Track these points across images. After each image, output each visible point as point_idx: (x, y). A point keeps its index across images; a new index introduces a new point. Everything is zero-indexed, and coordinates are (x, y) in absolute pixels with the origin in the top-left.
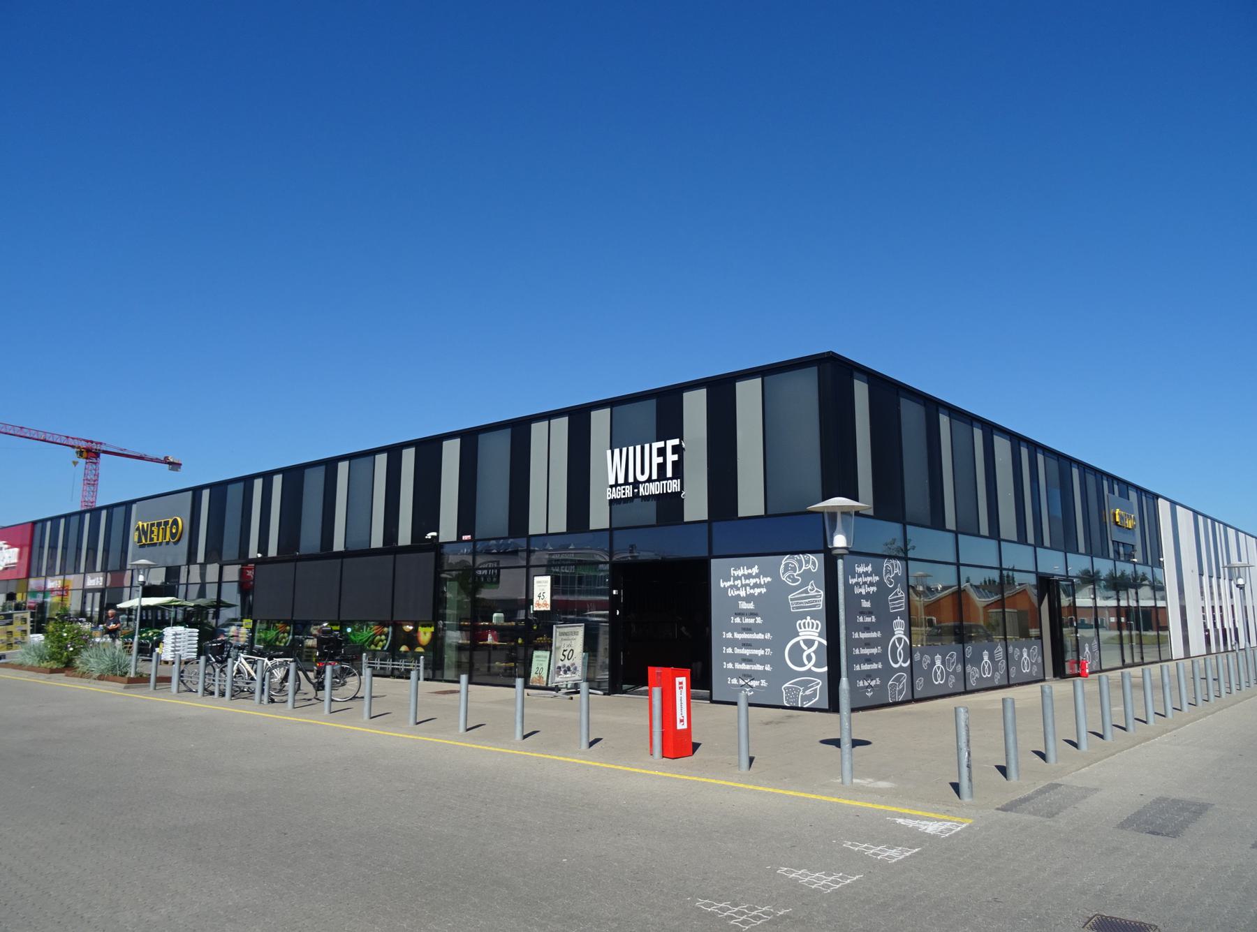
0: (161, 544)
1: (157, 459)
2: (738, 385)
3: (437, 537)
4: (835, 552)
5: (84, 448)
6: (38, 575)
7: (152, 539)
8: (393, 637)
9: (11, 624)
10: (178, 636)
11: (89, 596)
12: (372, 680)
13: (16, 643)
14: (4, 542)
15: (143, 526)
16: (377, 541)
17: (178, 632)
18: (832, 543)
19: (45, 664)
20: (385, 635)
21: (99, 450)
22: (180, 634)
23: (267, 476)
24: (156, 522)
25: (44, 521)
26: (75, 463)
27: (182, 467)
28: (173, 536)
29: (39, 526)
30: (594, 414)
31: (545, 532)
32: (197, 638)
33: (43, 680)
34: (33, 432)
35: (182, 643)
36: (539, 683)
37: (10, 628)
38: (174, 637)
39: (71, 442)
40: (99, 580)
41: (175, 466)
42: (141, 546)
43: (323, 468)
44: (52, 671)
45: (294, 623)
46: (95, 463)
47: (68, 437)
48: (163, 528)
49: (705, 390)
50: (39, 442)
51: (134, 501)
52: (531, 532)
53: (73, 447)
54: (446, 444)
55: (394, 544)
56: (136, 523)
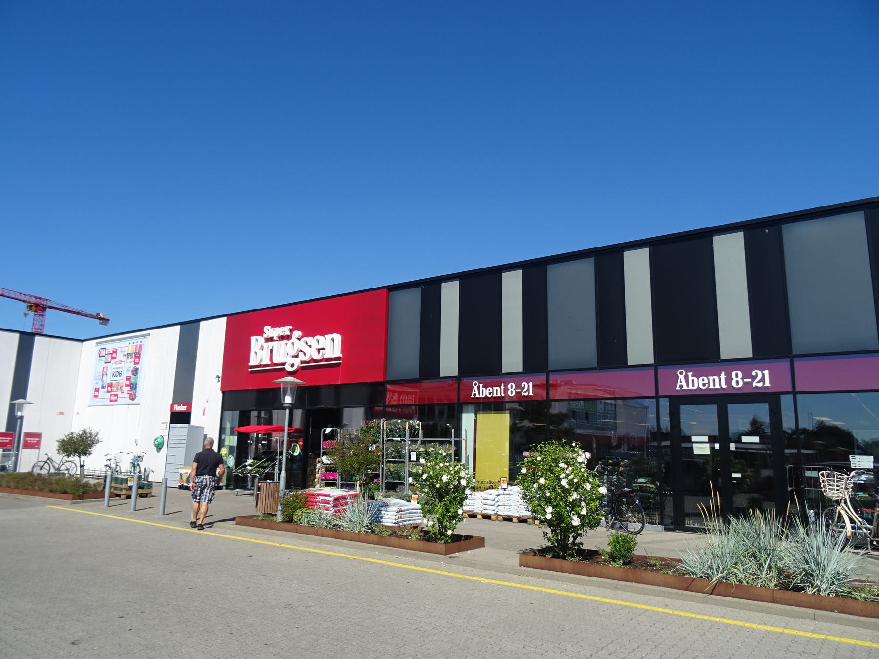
1: (91, 315)
4: (285, 405)
5: (33, 303)
21: (46, 305)
26: (26, 315)
27: (109, 322)
39: (23, 298)
46: (42, 316)
47: (21, 293)
53: (25, 301)
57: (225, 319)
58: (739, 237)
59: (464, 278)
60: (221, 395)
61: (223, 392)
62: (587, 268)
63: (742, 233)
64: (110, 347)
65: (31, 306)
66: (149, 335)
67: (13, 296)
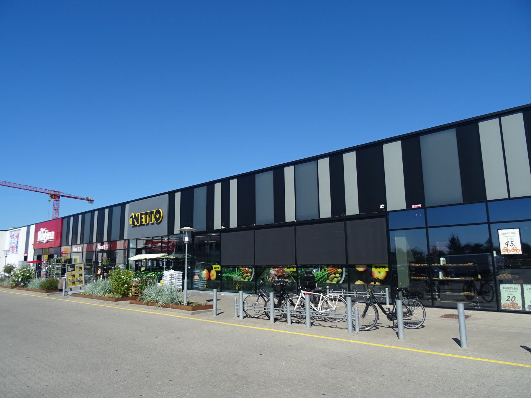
0: (148, 225)
1: (84, 198)
2: (384, 146)
3: (386, 207)
4: (185, 242)
5: (53, 194)
6: (67, 244)
7: (142, 222)
8: (255, 274)
9: (74, 270)
10: (172, 276)
11: (100, 255)
12: (217, 293)
13: (77, 281)
14: (46, 229)
15: (135, 215)
16: (326, 212)
17: (173, 274)
18: (184, 240)
19: (107, 295)
20: (339, 274)
21: (59, 195)
22: (173, 275)
23: (225, 182)
24: (149, 212)
25: (69, 217)
26: (49, 201)
27: (94, 202)
28: (157, 219)
29: (65, 221)
30: (345, 155)
31: (506, 197)
32: (182, 277)
33: (111, 306)
34: (35, 188)
35: (175, 280)
36: (513, 308)
37: (73, 273)
38: (170, 276)
39: (47, 192)
40: (79, 248)
41: (91, 201)
42: (133, 227)
43: (205, 187)
44: (117, 300)
45: (256, 267)
46: (58, 201)
47: (46, 190)
48: (149, 216)
49: (355, 152)
50: (34, 192)
51: (128, 203)
52: (488, 199)
53: (48, 194)
54: (216, 185)
55: (343, 214)
56: (130, 213)
57: (35, 225)
58: (398, 144)
59: (239, 177)
60: (33, 250)
61: (34, 250)
62: (451, 136)
63: (522, 113)
64: (13, 233)
65: (52, 196)
66: (20, 229)
67: (42, 191)
